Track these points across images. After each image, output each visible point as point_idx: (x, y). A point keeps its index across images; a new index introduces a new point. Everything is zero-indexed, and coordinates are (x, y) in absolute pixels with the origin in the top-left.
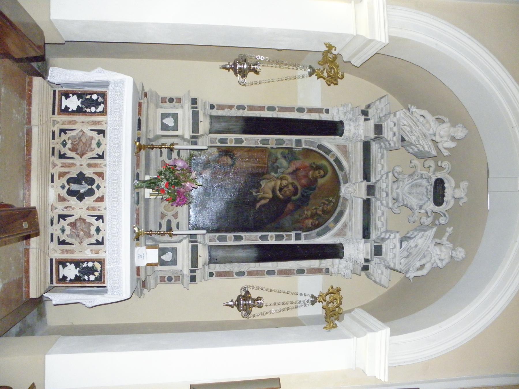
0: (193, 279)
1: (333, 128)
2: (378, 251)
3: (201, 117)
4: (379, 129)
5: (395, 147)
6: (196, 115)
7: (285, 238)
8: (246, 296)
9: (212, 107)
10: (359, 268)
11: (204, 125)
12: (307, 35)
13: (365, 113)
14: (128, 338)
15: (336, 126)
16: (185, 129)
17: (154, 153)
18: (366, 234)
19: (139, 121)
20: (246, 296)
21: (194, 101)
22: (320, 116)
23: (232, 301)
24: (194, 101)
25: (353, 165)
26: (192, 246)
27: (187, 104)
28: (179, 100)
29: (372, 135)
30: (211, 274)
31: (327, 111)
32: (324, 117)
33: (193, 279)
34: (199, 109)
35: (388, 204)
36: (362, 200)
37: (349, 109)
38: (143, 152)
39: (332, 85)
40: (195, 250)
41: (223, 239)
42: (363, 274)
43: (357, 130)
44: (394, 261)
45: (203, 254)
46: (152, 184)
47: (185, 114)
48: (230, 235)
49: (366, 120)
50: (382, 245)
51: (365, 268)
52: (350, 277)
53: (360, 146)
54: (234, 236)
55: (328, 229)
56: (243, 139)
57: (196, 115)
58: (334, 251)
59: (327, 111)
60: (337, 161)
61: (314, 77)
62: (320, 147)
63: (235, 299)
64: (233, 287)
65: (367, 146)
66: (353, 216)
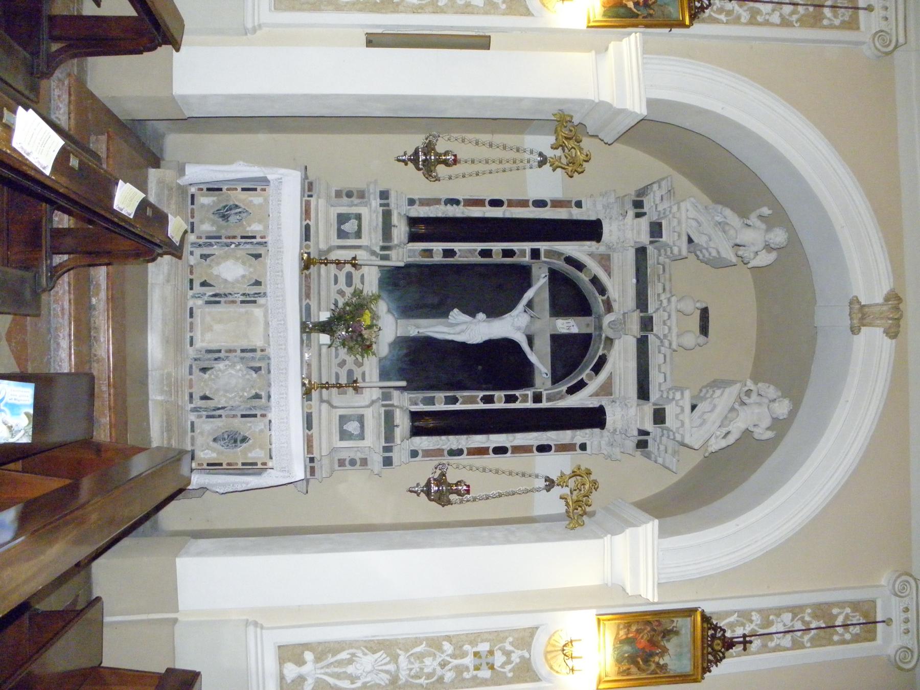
0: (388, 462)
1: (590, 230)
2: (659, 417)
3: (395, 220)
4: (656, 230)
5: (680, 255)
6: (387, 215)
7: (520, 399)
8: (441, 480)
9: (411, 202)
10: (631, 444)
11: (400, 231)
12: (540, 102)
13: (638, 204)
14: (378, 111)
15: (413, 362)
16: (372, 237)
17: (326, 272)
18: (643, 393)
19: (307, 228)
20: (441, 480)
21: (384, 195)
22: (571, 214)
23: (418, 485)
24: (384, 195)
25: (620, 287)
26: (385, 411)
27: (375, 202)
28: (362, 195)
29: (644, 238)
30: (414, 454)
31: (579, 204)
32: (576, 214)
33: (388, 462)
34: (393, 206)
35: (670, 344)
36: (635, 340)
37: (612, 200)
38: (313, 269)
39: (576, 174)
40: (389, 417)
41: (431, 401)
42: (638, 453)
43: (622, 232)
44: (681, 432)
45: (403, 423)
46: (324, 327)
47: (371, 214)
48: (440, 395)
49: (638, 215)
50: (664, 409)
51: (642, 445)
52: (619, 458)
53: (631, 255)
54: (445, 397)
55: (581, 385)
56: (456, 249)
57: (387, 215)
58: (593, 418)
59: (579, 204)
60: (595, 281)
61: (547, 167)
62: (570, 260)
63: (423, 483)
64: (425, 470)
65: (641, 252)
66: (621, 361)
